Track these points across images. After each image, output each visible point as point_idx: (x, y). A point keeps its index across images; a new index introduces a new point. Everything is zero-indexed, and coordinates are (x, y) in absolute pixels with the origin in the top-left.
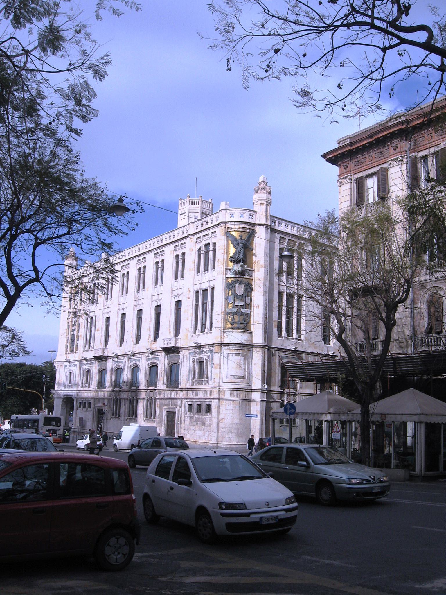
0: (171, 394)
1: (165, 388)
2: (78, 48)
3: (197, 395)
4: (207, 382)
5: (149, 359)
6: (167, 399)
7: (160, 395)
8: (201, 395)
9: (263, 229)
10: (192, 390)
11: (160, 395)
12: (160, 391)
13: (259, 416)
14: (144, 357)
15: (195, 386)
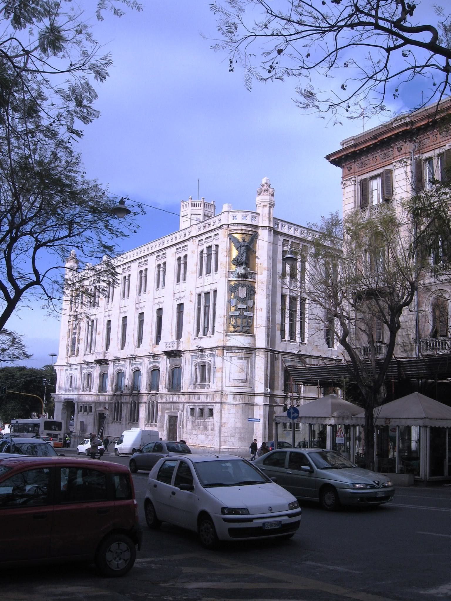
0: (173, 398)
1: (167, 391)
2: (79, 48)
3: (199, 399)
4: (209, 386)
5: (150, 363)
6: (168, 403)
7: (162, 399)
8: (203, 399)
9: (266, 231)
10: (194, 393)
11: (162, 399)
12: (162, 395)
13: (262, 420)
14: (146, 360)
15: (197, 390)
